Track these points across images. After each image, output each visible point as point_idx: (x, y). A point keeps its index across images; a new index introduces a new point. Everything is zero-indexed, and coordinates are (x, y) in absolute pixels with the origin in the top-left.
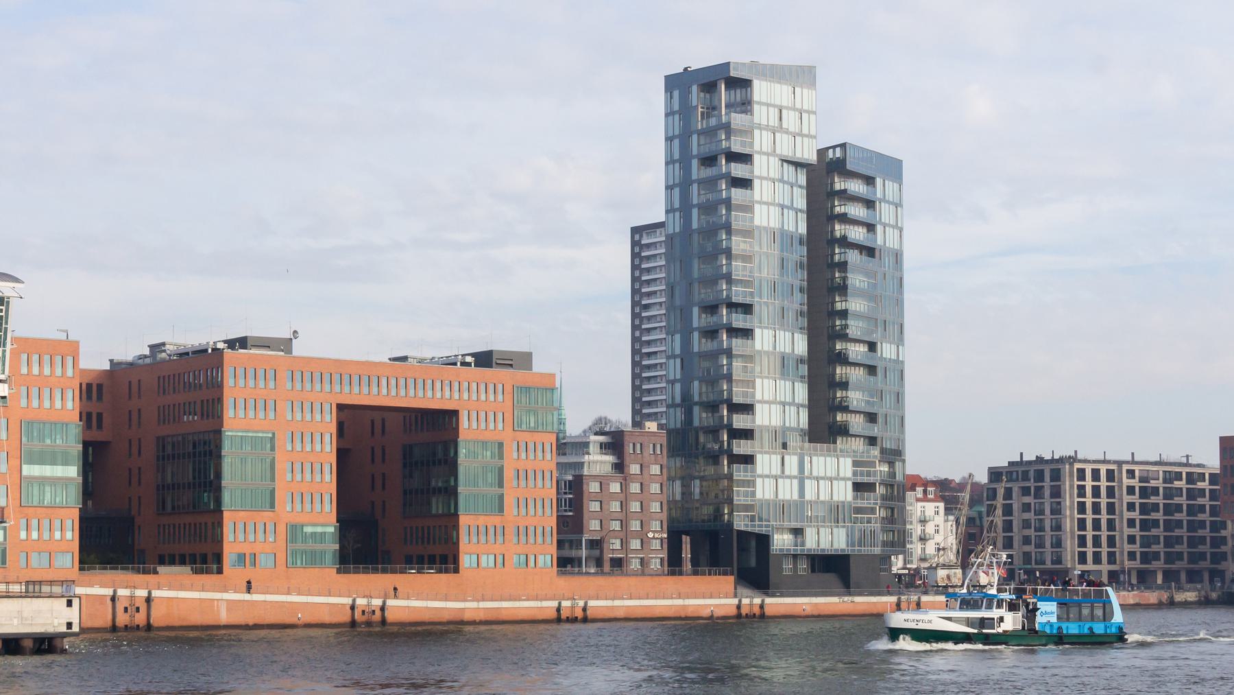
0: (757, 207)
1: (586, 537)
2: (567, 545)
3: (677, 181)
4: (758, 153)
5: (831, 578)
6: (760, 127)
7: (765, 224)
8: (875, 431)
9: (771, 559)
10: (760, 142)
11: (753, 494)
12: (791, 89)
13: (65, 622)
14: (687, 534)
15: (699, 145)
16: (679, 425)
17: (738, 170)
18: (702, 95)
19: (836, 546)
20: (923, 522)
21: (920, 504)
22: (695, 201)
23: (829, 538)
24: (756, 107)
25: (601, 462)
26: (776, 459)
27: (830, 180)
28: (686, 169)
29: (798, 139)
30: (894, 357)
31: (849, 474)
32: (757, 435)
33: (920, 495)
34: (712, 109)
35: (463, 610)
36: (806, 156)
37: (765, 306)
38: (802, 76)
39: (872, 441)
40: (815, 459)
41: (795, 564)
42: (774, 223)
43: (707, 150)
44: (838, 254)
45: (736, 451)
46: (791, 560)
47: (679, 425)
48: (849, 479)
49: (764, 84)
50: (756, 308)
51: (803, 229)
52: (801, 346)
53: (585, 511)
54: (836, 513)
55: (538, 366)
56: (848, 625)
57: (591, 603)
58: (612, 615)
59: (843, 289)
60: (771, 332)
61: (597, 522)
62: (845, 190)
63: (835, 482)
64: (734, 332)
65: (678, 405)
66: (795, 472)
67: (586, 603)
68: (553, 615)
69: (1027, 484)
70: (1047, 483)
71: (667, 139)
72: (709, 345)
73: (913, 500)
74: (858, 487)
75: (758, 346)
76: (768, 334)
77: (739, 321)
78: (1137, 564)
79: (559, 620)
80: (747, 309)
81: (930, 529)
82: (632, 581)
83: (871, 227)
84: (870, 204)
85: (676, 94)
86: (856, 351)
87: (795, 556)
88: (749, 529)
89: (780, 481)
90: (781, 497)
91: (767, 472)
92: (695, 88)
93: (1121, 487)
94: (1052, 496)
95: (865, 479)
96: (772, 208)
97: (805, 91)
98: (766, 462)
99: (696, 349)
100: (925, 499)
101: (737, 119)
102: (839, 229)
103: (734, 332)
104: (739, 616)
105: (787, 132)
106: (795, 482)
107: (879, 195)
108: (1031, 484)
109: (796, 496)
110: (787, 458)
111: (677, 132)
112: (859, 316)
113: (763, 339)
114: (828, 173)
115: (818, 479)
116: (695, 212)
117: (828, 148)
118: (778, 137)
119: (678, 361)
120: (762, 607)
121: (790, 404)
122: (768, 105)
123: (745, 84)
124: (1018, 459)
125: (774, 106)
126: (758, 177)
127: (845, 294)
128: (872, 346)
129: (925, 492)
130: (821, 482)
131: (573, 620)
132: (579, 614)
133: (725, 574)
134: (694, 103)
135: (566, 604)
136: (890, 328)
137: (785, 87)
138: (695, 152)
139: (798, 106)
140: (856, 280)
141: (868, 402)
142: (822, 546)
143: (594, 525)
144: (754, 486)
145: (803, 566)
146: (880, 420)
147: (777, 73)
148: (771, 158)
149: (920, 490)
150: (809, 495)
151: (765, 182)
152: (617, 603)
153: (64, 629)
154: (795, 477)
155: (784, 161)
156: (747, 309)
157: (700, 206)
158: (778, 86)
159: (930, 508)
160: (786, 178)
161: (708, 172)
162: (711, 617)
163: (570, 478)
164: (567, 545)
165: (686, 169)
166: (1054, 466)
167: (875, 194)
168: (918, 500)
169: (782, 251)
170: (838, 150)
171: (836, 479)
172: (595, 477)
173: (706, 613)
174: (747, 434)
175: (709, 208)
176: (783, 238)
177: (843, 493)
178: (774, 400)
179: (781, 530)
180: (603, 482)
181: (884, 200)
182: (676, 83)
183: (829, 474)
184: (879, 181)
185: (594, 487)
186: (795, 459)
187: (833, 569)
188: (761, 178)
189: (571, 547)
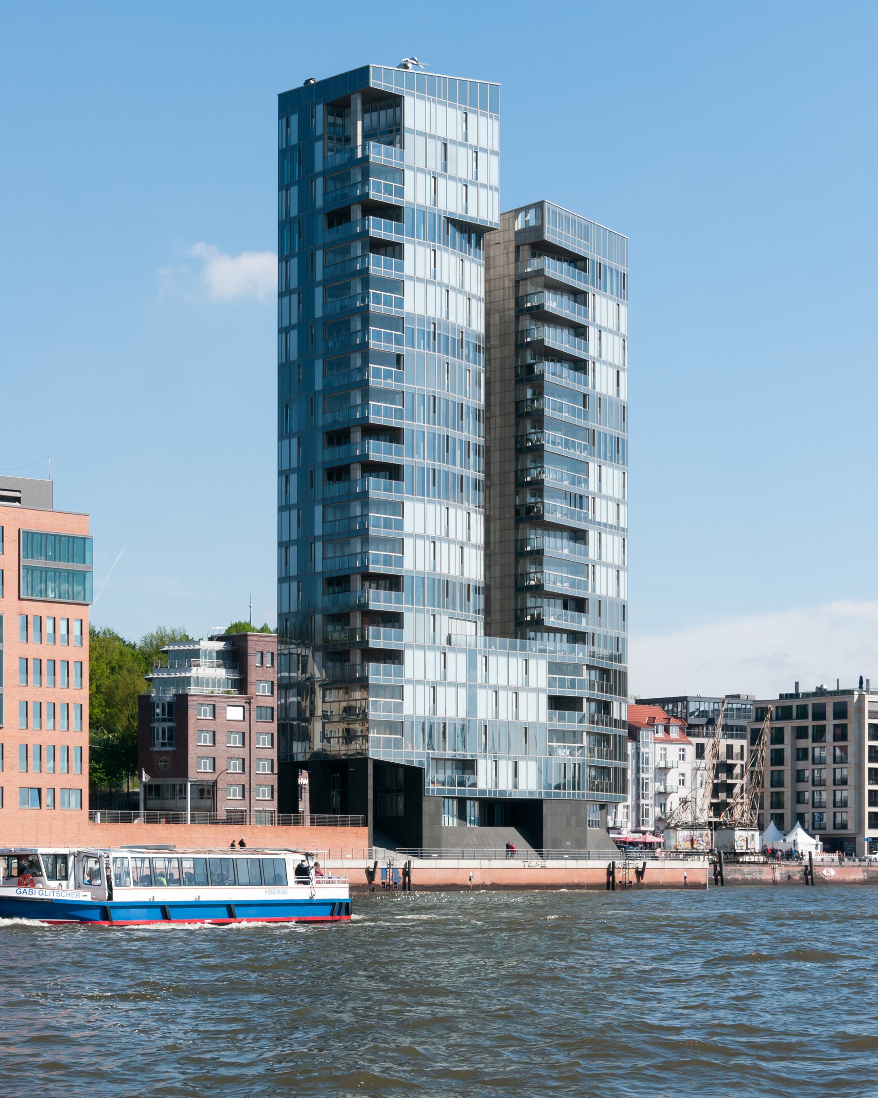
5: (511, 834)
12: (460, 115)
18: (331, 119)
21: (659, 746)
24: (408, 137)
31: (543, 683)
40: (492, 660)
43: (337, 566)
49: (420, 103)
66: (462, 678)
69: (802, 723)
70: (830, 723)
71: (280, 544)
74: (557, 703)
80: (394, 435)
84: (579, 331)
85: (294, 119)
89: (440, 690)
92: (320, 109)
95: (568, 692)
97: (483, 120)
108: (809, 723)
109: (462, 714)
111: (294, 537)
116: (319, 292)
124: (793, 691)
127: (541, 564)
133: (355, 824)
137: (452, 112)
138: (320, 424)
146: (592, 607)
150: (484, 712)
151: (420, 543)
154: (462, 685)
156: (394, 435)
157: (326, 174)
158: (441, 109)
165: (306, 302)
166: (839, 699)
168: (657, 741)
177: (535, 710)
182: (290, 103)
188: (414, 682)
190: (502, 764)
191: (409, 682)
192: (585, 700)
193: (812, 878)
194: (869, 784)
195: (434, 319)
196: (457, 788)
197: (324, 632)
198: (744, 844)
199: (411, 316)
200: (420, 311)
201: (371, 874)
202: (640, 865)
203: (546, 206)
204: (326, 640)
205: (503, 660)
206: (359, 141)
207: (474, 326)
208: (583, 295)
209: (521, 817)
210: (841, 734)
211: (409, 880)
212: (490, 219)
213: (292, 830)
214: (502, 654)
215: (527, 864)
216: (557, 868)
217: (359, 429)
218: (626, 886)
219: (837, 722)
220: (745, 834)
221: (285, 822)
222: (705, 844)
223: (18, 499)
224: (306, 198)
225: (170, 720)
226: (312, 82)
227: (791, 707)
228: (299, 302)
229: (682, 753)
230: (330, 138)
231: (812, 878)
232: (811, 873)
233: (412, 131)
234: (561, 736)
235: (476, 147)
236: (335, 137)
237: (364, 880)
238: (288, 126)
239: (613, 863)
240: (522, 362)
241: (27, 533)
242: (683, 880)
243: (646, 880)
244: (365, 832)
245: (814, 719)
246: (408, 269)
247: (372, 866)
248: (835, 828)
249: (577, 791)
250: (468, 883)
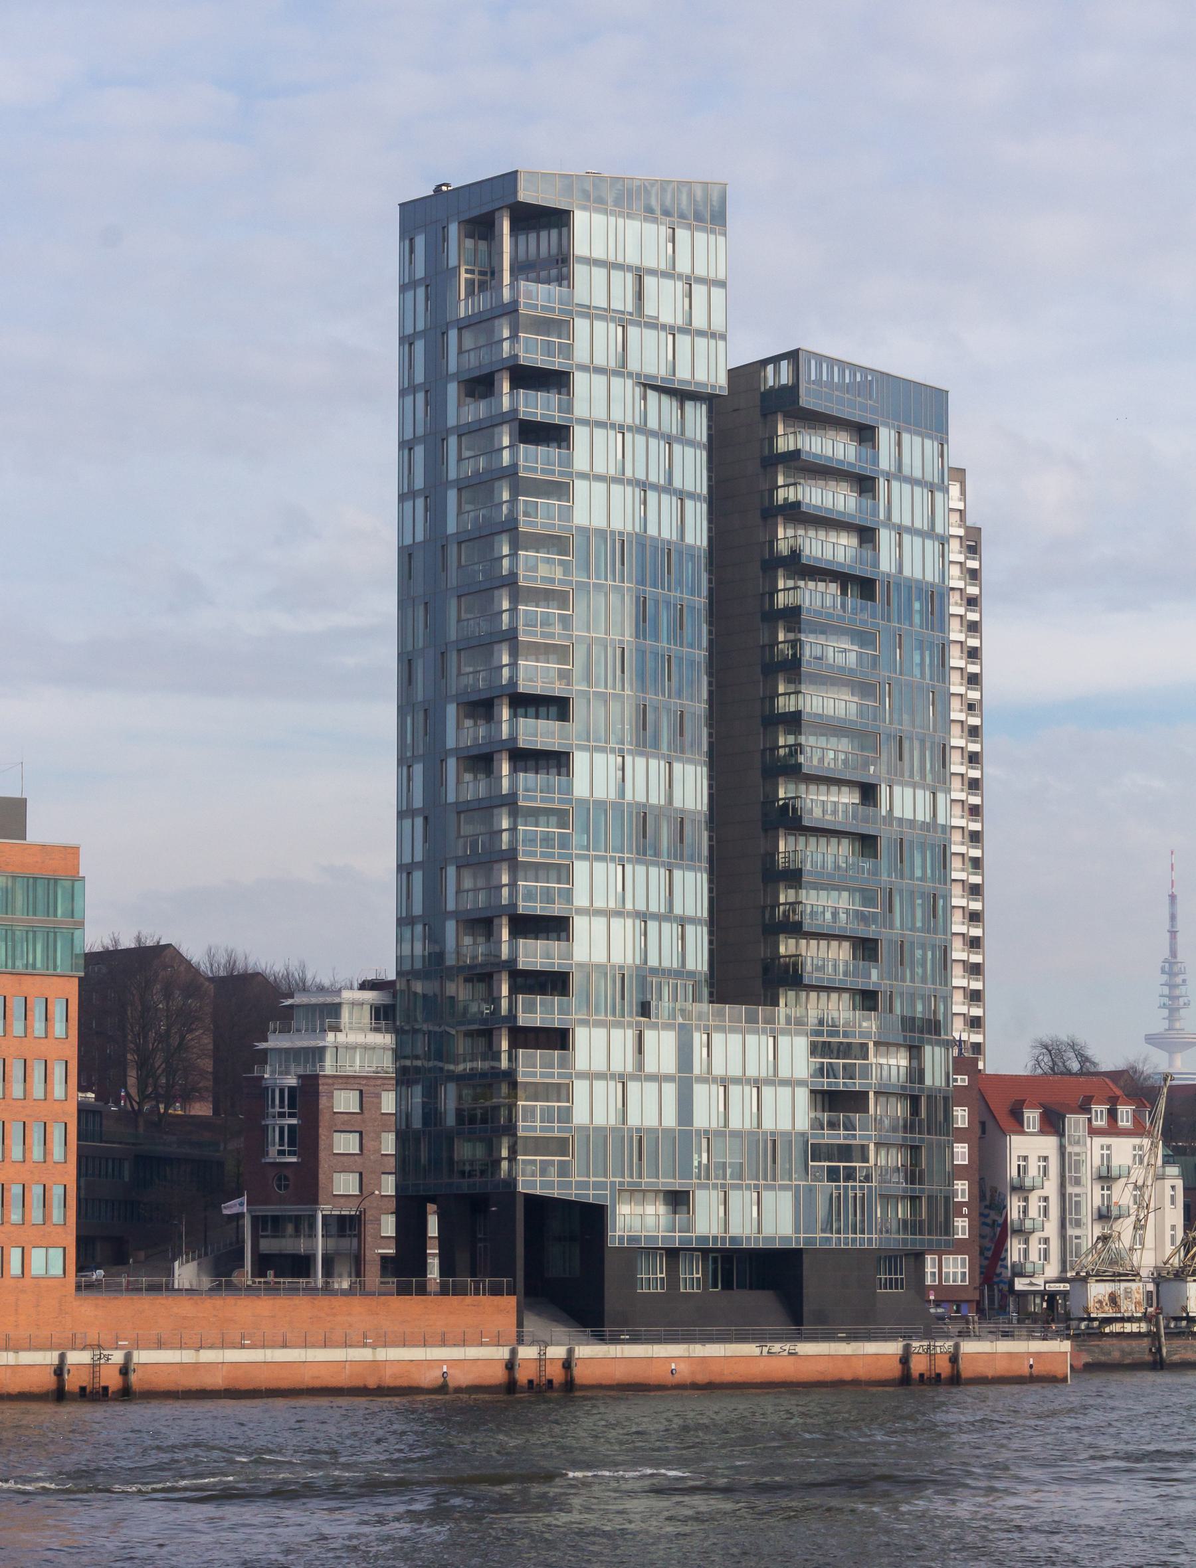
0: (580, 486)
1: (325, 1209)
2: (290, 1228)
3: (420, 431)
4: (584, 368)
5: (765, 1300)
6: (589, 312)
7: (599, 522)
8: (874, 977)
9: (608, 1257)
10: (592, 342)
11: (566, 1115)
12: (664, 231)
14: (433, 1200)
17: (538, 406)
18: (469, 243)
19: (768, 1230)
20: (1106, 1178)
21: (1098, 1141)
22: (452, 475)
23: (767, 1216)
24: (580, 272)
25: (366, 1048)
26: (623, 1038)
27: (754, 428)
28: (435, 405)
30: (923, 815)
32: (576, 982)
33: (1100, 1123)
34: (488, 277)
35: (196, 1366)
36: (701, 376)
37: (604, 700)
39: (868, 999)
40: (717, 1038)
41: (672, 1271)
42: (622, 521)
43: (474, 362)
44: (788, 592)
45: (523, 1019)
46: (661, 1263)
48: (801, 1083)
49: (599, 219)
50: (578, 709)
51: (697, 534)
52: (691, 788)
53: (322, 1155)
54: (763, 1155)
56: (770, 1410)
57: (142, 1357)
58: (193, 1382)
59: (792, 668)
60: (614, 760)
61: (353, 1179)
62: (797, 452)
63: (767, 1091)
64: (526, 759)
66: (669, 1065)
67: (128, 1357)
68: (48, 1381)
72: (474, 788)
73: (1082, 1131)
75: (580, 788)
76: (605, 764)
77: (537, 733)
79: (59, 1395)
80: (559, 707)
81: (1122, 1195)
82: (184, 1307)
83: (866, 535)
85: (420, 241)
86: (826, 804)
87: (673, 1254)
88: (555, 1193)
89: (633, 1086)
90: (633, 1120)
91: (599, 1065)
92: (453, 229)
95: (841, 1084)
96: (616, 489)
98: (596, 1045)
99: (451, 798)
100: (1113, 1129)
101: (537, 296)
102: (785, 536)
103: (526, 759)
104: (511, 1386)
105: (654, 325)
106: (670, 1090)
107: (885, 462)
110: (650, 1036)
112: (832, 728)
113: (593, 776)
114: (764, 415)
115: (725, 1082)
117: (764, 363)
118: (645, 329)
119: (419, 821)
120: (567, 1364)
121: (659, 917)
122: (609, 266)
123: (558, 219)
126: (584, 422)
128: (868, 793)
129: (1112, 1115)
130: (734, 1090)
131: (94, 1395)
132: (111, 1379)
133: (496, 1291)
134: (453, 262)
135: (76, 1358)
136: (913, 753)
138: (453, 368)
139: (683, 267)
140: (831, 650)
141: (862, 917)
142: (735, 1231)
143: (345, 1184)
144: (569, 1097)
145: (692, 1275)
146: (883, 950)
147: (627, 197)
148: (616, 382)
149: (1100, 1109)
150: (702, 1118)
152: (207, 1356)
154: (668, 1078)
155: (648, 385)
156: (559, 707)
159: (1123, 1150)
160: (653, 424)
161: (477, 410)
162: (443, 1388)
163: (292, 1081)
164: (290, 1228)
165: (435, 405)
167: (875, 460)
168: (1094, 1132)
169: (642, 582)
171: (770, 1082)
172: (347, 1081)
173: (430, 1378)
174: (555, 983)
175: (479, 487)
176: (649, 558)
177: (791, 1113)
178: (625, 913)
179: (636, 1193)
180: (365, 1087)
181: (898, 474)
183: (752, 1072)
184: (885, 436)
185: (345, 1101)
186: (669, 1039)
187: (765, 1282)
188: (591, 1076)
189: (297, 1232)
191: (583, 1075)
192: (871, 1095)
195: (621, 534)
196: (677, 1234)
205: (735, 1039)
206: (507, 278)
207: (689, 539)
212: (712, 380)
213: (412, 1303)
214: (733, 1030)
215: (765, 1350)
216: (817, 1355)
217: (506, 701)
221: (403, 1290)
225: (291, 1115)
226: (444, 188)
228: (426, 511)
229: (1105, 1152)
233: (591, 262)
235: (688, 278)
236: (476, 270)
238: (412, 251)
246: (580, 462)
249: (850, 1236)
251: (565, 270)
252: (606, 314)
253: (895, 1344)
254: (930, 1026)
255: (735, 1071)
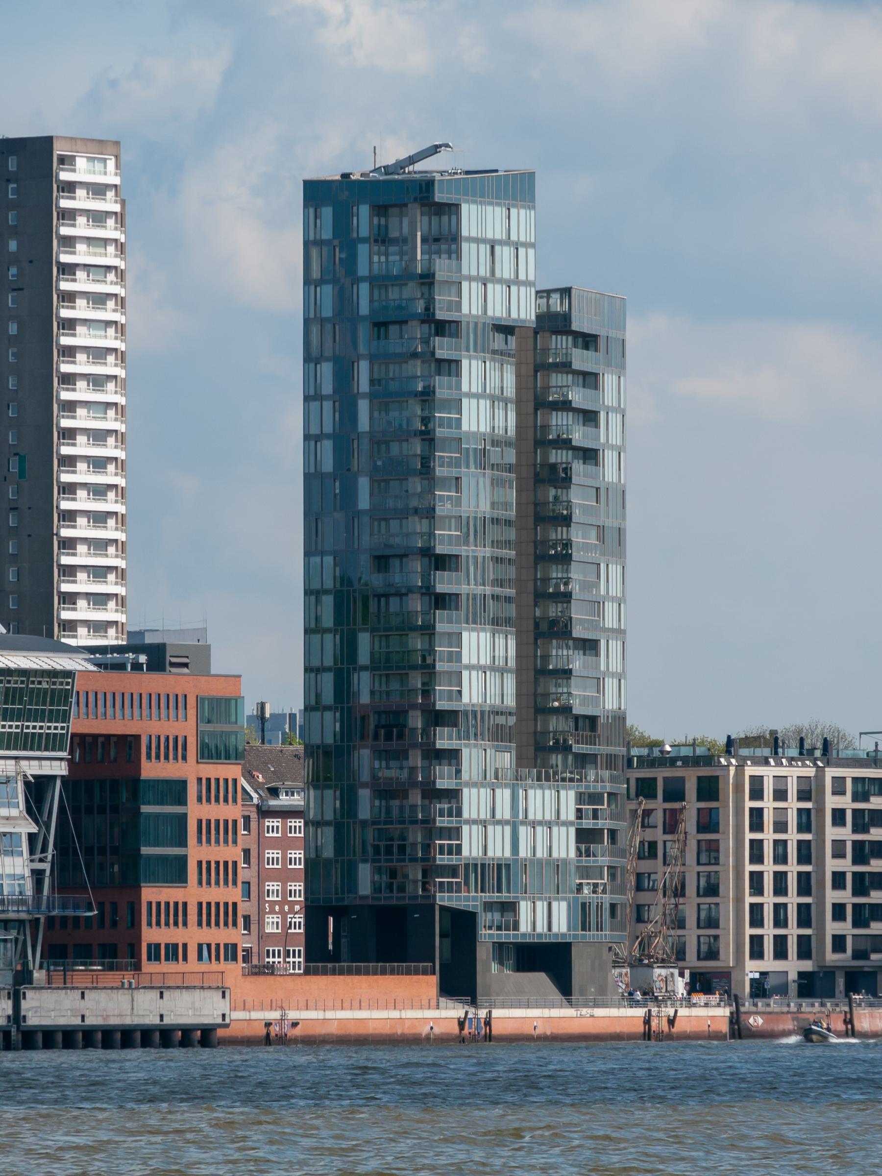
5: (541, 978)
13: (220, 1013)
15: (371, 301)
16: (329, 740)
29: (514, 289)
38: (516, 189)
47: (329, 740)
48: (571, 823)
49: (473, 207)
55: (221, 663)
65: (327, 708)
70: (692, 806)
78: (845, 958)
91: (474, 816)
93: (821, 810)
94: (702, 827)
97: (522, 212)
106: (508, 829)
109: (508, 854)
115: (534, 824)
116: (363, 406)
125: (484, 241)
130: (539, 829)
133: (425, 972)
137: (498, 209)
144: (459, 837)
152: (330, 1015)
153: (219, 1021)
154: (507, 822)
158: (490, 209)
170: (556, 297)
177: (564, 845)
190: (539, 904)
192: (606, 831)
193: (739, 1029)
194: (751, 895)
197: (373, 771)
198: (663, 985)
199: (468, 433)
200: (474, 428)
201: (461, 1024)
202: (671, 1012)
203: (573, 292)
204: (374, 777)
208: (593, 377)
209: (548, 960)
210: (709, 823)
211: (853, 1027)
218: (661, 1037)
219: (702, 805)
220: (663, 972)
222: (624, 987)
223: (186, 665)
224: (344, 303)
227: (655, 779)
230: (376, 241)
231: (739, 1029)
232: (738, 1022)
233: (470, 240)
234: (585, 872)
235: (517, 243)
237: (456, 1030)
239: (650, 1011)
240: (547, 465)
241: (211, 700)
242: (706, 1028)
243: (678, 1028)
244: (433, 980)
245: (665, 800)
247: (463, 1016)
248: (699, 959)
250: (533, 1032)
251: (454, 247)
252: (477, 278)
253: (641, 1009)
254: (14, 697)
255: (539, 817)
